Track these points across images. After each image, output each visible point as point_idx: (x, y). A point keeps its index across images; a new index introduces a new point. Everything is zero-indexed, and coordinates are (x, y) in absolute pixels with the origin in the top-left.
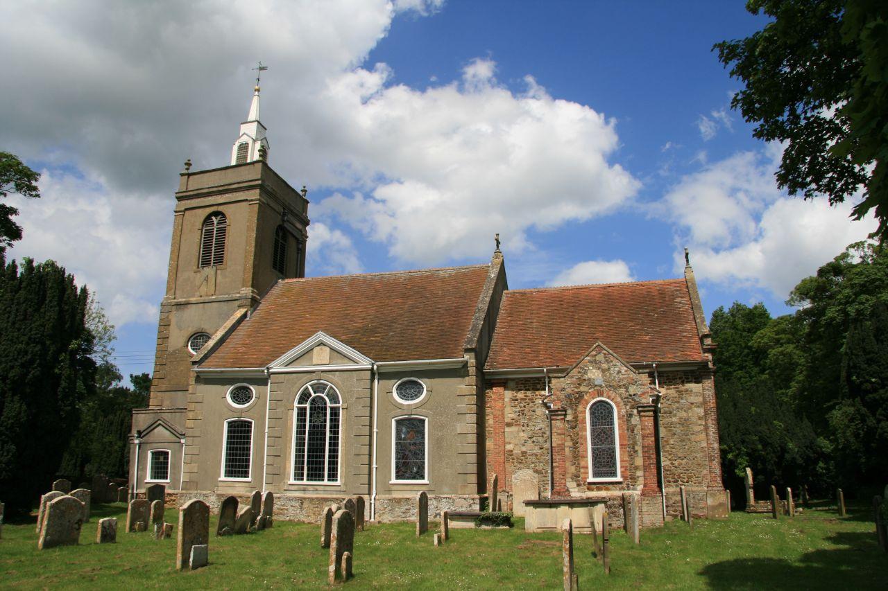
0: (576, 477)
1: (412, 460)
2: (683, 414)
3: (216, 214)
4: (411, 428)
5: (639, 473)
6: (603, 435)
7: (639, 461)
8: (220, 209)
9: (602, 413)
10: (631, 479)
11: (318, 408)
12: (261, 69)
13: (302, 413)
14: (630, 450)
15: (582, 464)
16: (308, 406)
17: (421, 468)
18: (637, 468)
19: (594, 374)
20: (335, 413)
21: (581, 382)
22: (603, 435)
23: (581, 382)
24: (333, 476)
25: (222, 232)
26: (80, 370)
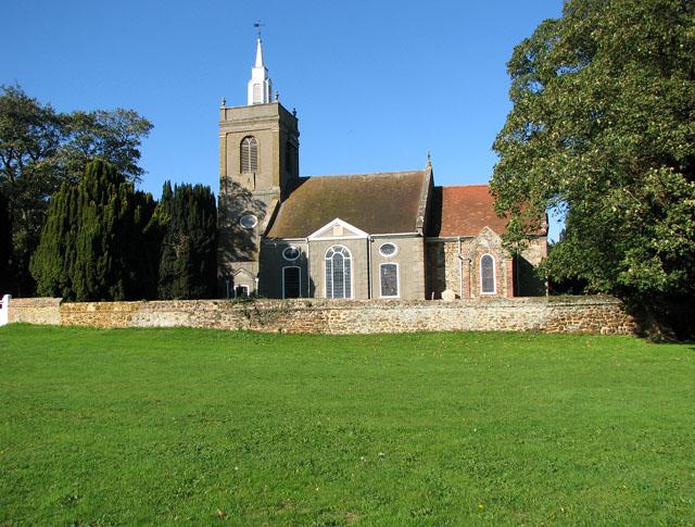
1: (390, 286)
2: (668, 220)
3: (249, 137)
4: (390, 270)
6: (487, 272)
7: (505, 284)
9: (487, 262)
11: (338, 259)
12: (257, 25)
13: (328, 263)
14: (501, 278)
16: (331, 258)
17: (395, 290)
19: (484, 243)
20: (348, 263)
21: (478, 245)
22: (487, 272)
23: (478, 245)
24: (348, 295)
25: (254, 150)
26: (680, 288)
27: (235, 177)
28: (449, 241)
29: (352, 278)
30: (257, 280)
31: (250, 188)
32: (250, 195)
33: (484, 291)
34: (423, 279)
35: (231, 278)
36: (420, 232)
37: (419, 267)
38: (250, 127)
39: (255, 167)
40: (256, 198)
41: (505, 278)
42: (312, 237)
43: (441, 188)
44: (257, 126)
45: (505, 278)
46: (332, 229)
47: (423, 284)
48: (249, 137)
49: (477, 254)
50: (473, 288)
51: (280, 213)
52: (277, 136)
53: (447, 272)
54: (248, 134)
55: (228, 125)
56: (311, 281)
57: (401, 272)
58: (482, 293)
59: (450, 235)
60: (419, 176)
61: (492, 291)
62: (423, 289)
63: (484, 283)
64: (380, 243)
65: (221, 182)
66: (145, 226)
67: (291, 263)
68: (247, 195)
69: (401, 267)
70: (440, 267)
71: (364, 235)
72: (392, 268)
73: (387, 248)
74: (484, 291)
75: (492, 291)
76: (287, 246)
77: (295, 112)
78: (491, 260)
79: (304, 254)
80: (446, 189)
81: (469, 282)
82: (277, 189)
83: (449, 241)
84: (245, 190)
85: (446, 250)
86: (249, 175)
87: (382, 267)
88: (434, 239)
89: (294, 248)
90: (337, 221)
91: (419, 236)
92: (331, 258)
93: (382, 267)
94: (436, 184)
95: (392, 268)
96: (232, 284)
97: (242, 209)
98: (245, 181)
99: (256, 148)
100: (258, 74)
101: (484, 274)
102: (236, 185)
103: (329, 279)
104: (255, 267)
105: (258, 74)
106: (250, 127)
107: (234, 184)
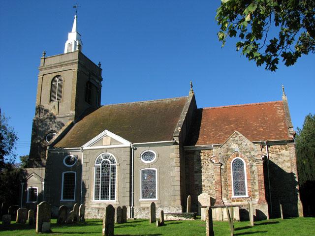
0: (226, 195)
3: (58, 76)
5: (257, 193)
6: (238, 175)
7: (257, 187)
8: (60, 74)
9: (238, 165)
10: (252, 196)
11: (105, 166)
13: (98, 169)
15: (229, 189)
16: (100, 165)
17: (154, 193)
18: (255, 191)
19: (234, 147)
20: (114, 169)
22: (238, 175)
23: (228, 150)
25: (61, 86)
27: (46, 105)
28: (205, 149)
29: (116, 181)
30: (43, 183)
31: (54, 112)
32: (55, 118)
33: (235, 194)
34: (179, 183)
35: (25, 181)
36: (177, 139)
37: (175, 172)
38: (59, 69)
39: (60, 97)
40: (58, 120)
41: (256, 181)
42: (85, 147)
43: (202, 109)
44: (63, 68)
45: (256, 181)
46: (101, 139)
47: (179, 188)
48: (58, 76)
49: (227, 158)
50: (224, 192)
51: (71, 130)
52: (76, 73)
53: (203, 177)
54: (57, 74)
55: (44, 69)
56: (83, 183)
57: (159, 178)
58: (233, 196)
59: (205, 143)
60: (184, 101)
61: (244, 194)
62: (179, 193)
63: (236, 187)
64: (141, 150)
65: (37, 109)
66: (282, 206)
67: (68, 169)
68: (52, 118)
69: (159, 173)
70: (196, 172)
71: (127, 143)
72: (151, 174)
73: (148, 155)
74: (235, 194)
75: (244, 194)
76: (67, 154)
77: (100, 65)
78: (242, 164)
79: (80, 161)
80: (205, 110)
81: (221, 185)
82: (73, 112)
83: (205, 149)
84: (52, 114)
85: (202, 158)
86: (55, 103)
87: (143, 172)
88: (191, 148)
89: (72, 156)
90: (107, 132)
91: (175, 143)
92: (100, 165)
93: (143, 172)
94: (199, 107)
95: (151, 174)
96: (26, 186)
97: (48, 129)
98: (52, 108)
99: (61, 83)
100: (72, 37)
101: (236, 176)
102: (47, 111)
103: (97, 183)
104: (42, 172)
105: (72, 37)
106: (59, 69)
107: (45, 110)
